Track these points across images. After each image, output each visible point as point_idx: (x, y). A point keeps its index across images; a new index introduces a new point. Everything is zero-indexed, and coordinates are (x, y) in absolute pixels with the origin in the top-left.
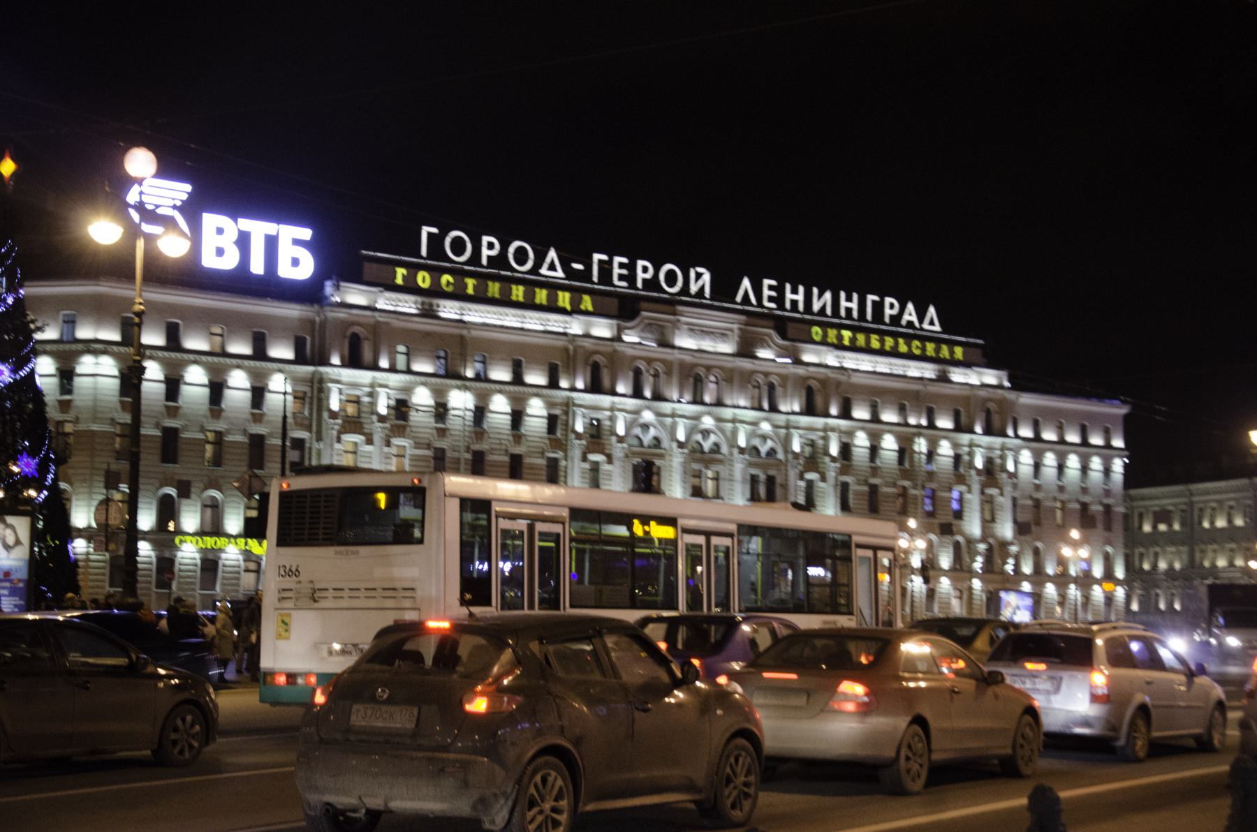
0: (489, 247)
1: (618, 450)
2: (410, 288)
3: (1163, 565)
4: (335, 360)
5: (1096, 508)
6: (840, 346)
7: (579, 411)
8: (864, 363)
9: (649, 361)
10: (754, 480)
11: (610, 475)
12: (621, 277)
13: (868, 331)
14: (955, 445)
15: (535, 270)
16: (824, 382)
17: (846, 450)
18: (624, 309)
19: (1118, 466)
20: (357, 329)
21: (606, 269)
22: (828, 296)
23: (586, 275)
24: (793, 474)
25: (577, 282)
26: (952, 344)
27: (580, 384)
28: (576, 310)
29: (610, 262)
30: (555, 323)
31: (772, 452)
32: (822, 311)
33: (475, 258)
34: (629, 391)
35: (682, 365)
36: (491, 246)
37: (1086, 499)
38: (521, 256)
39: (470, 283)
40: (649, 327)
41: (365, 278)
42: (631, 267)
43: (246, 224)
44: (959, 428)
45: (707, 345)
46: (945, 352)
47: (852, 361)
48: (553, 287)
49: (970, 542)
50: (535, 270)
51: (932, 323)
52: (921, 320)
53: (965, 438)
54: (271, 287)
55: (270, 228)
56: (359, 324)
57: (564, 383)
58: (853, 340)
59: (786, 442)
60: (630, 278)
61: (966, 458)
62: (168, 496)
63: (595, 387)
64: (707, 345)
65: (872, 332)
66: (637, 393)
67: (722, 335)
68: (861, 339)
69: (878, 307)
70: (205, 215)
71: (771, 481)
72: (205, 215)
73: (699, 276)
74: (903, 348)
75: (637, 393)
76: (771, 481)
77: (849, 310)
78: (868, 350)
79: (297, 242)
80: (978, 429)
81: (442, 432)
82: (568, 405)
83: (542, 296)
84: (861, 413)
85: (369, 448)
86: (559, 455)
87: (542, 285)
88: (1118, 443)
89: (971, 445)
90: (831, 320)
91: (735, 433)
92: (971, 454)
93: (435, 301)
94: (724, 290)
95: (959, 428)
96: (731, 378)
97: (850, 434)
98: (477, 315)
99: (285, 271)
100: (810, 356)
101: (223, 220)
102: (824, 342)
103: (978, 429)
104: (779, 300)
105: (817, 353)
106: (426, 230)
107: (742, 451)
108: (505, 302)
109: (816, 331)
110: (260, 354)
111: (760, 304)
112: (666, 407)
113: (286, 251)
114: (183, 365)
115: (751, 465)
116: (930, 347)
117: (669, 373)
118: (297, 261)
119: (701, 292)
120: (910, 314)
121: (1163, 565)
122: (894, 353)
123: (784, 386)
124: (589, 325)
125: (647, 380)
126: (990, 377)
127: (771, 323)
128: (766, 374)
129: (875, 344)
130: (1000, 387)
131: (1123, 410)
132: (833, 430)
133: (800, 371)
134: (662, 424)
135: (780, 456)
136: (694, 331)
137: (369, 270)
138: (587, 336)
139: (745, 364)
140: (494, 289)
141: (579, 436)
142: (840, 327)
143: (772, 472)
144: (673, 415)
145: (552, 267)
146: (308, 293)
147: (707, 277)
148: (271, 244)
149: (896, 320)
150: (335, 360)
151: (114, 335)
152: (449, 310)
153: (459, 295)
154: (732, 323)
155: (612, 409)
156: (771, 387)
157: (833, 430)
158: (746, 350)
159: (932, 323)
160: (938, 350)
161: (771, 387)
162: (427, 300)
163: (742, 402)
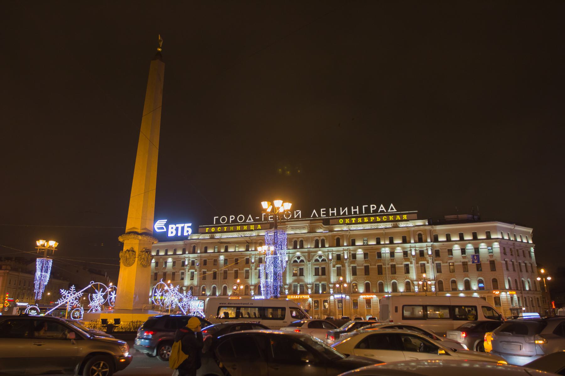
4: (412, 241)
7: (253, 257)
14: (403, 248)
15: (245, 221)
16: (343, 236)
22: (346, 209)
23: (260, 220)
28: (256, 229)
29: (369, 207)
30: (248, 234)
32: (344, 214)
36: (373, 207)
38: (241, 219)
43: (177, 225)
45: (298, 231)
46: (398, 217)
47: (353, 227)
48: (249, 225)
49: (412, 281)
52: (387, 209)
53: (408, 245)
55: (183, 225)
56: (420, 230)
57: (250, 250)
58: (356, 221)
61: (409, 252)
64: (298, 231)
67: (304, 228)
69: (368, 210)
71: (323, 269)
73: (297, 213)
76: (323, 269)
79: (188, 227)
93: (398, 223)
96: (308, 240)
98: (225, 236)
100: (337, 228)
104: (327, 214)
105: (340, 227)
106: (364, 206)
108: (235, 231)
109: (341, 221)
110: (462, 238)
113: (186, 229)
114: (465, 245)
115: (315, 265)
116: (391, 218)
120: (382, 208)
124: (259, 233)
126: (419, 223)
127: (322, 221)
130: (424, 225)
132: (345, 250)
136: (293, 228)
138: (259, 236)
142: (350, 218)
143: (323, 266)
145: (250, 219)
147: (300, 212)
148: (183, 228)
152: (217, 236)
154: (306, 224)
155: (328, 252)
157: (345, 250)
158: (312, 231)
162: (395, 223)
163: (291, 248)
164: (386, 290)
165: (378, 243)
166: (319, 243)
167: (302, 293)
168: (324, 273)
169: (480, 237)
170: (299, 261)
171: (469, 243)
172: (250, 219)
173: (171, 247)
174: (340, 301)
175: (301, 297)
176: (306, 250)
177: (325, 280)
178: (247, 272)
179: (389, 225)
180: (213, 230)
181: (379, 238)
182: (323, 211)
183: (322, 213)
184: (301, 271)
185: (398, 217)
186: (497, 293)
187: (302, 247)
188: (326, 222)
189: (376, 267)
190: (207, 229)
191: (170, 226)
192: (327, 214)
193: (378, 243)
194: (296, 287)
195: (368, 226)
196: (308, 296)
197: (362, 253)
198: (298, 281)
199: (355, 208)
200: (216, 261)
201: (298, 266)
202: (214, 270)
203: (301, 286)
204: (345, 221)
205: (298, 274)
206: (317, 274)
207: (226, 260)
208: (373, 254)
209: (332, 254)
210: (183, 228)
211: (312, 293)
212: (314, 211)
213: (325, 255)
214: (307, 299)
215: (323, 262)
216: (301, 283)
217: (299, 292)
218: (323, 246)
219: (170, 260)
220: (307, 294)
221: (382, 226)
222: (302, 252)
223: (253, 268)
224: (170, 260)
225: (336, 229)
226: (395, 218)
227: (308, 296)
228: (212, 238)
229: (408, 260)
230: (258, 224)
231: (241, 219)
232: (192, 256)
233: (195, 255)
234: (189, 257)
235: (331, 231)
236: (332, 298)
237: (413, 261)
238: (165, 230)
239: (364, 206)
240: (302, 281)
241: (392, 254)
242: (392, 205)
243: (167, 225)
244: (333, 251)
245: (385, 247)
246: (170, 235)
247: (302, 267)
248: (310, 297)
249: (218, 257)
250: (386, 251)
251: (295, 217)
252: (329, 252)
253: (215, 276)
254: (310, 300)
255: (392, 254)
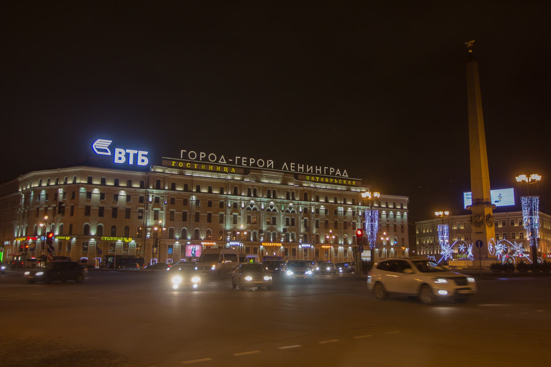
0: (202, 155)
1: (242, 212)
2: (176, 167)
3: (428, 242)
4: (151, 187)
5: (95, 208)
6: (315, 181)
8: (323, 186)
9: (253, 186)
10: (287, 219)
11: (240, 218)
12: (244, 163)
13: (325, 177)
14: (353, 209)
15: (217, 161)
16: (310, 191)
17: (317, 211)
18: (246, 172)
19: (405, 214)
20: (236, 185)
21: (240, 161)
23: (233, 163)
24: (300, 218)
25: (230, 165)
26: (352, 180)
27: (230, 193)
28: (230, 172)
30: (222, 176)
31: (293, 212)
33: (198, 158)
34: (246, 195)
35: (263, 187)
36: (203, 155)
37: (389, 223)
39: (196, 165)
40: (253, 176)
41: (163, 164)
42: (248, 160)
43: (128, 151)
44: (354, 204)
45: (272, 181)
47: (318, 186)
48: (222, 166)
49: (279, 233)
50: (217, 161)
51: (345, 174)
52: (342, 174)
53: (356, 207)
54: (135, 167)
55: (136, 152)
56: (158, 177)
57: (225, 193)
58: (320, 179)
59: (298, 208)
60: (248, 163)
62: (184, 229)
63: (235, 194)
64: (272, 181)
65: (326, 177)
66: (249, 195)
67: (277, 179)
68: (322, 179)
69: (328, 171)
70: (514, 204)
71: (293, 220)
72: (514, 204)
73: (270, 162)
74: (336, 181)
75: (288, 198)
76: (293, 220)
77: (318, 172)
78: (324, 182)
79: (143, 155)
80: (360, 204)
81: (395, 221)
82: (226, 199)
83: (218, 168)
84: (322, 200)
85: (162, 212)
86: (355, 221)
87: (219, 165)
88: (405, 207)
89: (358, 209)
90: (314, 174)
91: (261, 205)
92: (358, 211)
94: (278, 166)
95: (354, 204)
96: (281, 191)
97: (319, 206)
99: (140, 163)
101: (122, 151)
102: (310, 180)
103: (360, 204)
104: (296, 169)
106: (182, 151)
107: (283, 211)
108: (207, 170)
109: (308, 178)
111: (290, 169)
112: (258, 199)
113: (140, 158)
115: (286, 215)
116: (345, 182)
117: (259, 190)
118: (143, 160)
119: (270, 167)
120: (338, 172)
121: (428, 242)
122: (333, 183)
123: (259, 190)
124: (234, 176)
125: (253, 192)
127: (293, 175)
128: (291, 190)
129: (327, 180)
131: (407, 199)
132: (313, 205)
133: (301, 188)
134: (257, 205)
135: (296, 213)
136: (267, 178)
137: (164, 162)
138: (315, 187)
139: (284, 187)
140: (203, 167)
141: (229, 208)
143: (293, 217)
144: (260, 201)
146: (146, 169)
147: (272, 163)
148: (136, 156)
149: (334, 174)
150: (151, 187)
151: (85, 182)
152: (188, 173)
153: (192, 169)
154: (280, 175)
155: (240, 200)
156: (293, 193)
157: (313, 205)
158: (284, 183)
159: (345, 174)
160: (347, 182)
161: (293, 193)
163: (283, 198)
164: (340, 243)
165: (336, 202)
166: (290, 195)
167: (274, 241)
168: (293, 224)
169: (122, 184)
170: (272, 210)
171: (123, 190)
172: (222, 160)
173: (124, 178)
174: (306, 249)
175: (275, 244)
176: (279, 201)
177: (294, 230)
178: (222, 216)
179: (344, 188)
180: (181, 165)
181: (105, 179)
182: (293, 165)
183: (243, 161)
184: (274, 219)
185: (349, 182)
186: (404, 248)
187: (275, 197)
188: (296, 176)
189: (182, 213)
190: (174, 162)
191: (117, 150)
192: (296, 169)
193: (336, 202)
194: (269, 234)
195: (329, 186)
196: (281, 244)
197: (85, 191)
198: (271, 229)
199: (318, 168)
200: (186, 202)
201: (271, 215)
202: (184, 211)
203: (274, 234)
204: (311, 178)
205: (271, 223)
206: (287, 224)
207: (197, 201)
208: (332, 210)
209: (153, 196)
210: (136, 156)
211: (192, 239)
212: (285, 164)
213: (295, 207)
214: (280, 247)
215: (293, 214)
216: (274, 232)
217: (271, 240)
218: (294, 199)
219: (123, 193)
220: (280, 242)
221: (339, 188)
222: (275, 202)
223: (229, 212)
224: (123, 193)
225: (304, 185)
226: (347, 182)
227: (281, 244)
228: (182, 174)
229: (355, 219)
230: (354, 180)
231: (212, 157)
232: (155, 191)
233: (162, 192)
234: (153, 193)
235: (301, 186)
236: (300, 247)
237: (164, 209)
238: (109, 153)
239: (182, 151)
240: (276, 230)
241: (345, 212)
242: (223, 156)
243: (112, 148)
244: (244, 200)
245: (341, 206)
246: (117, 161)
247: (274, 216)
248: (283, 245)
249: (189, 197)
250: (341, 209)
251: (268, 166)
252: (298, 205)
253: (184, 217)
254: (282, 247)
255: (345, 212)
